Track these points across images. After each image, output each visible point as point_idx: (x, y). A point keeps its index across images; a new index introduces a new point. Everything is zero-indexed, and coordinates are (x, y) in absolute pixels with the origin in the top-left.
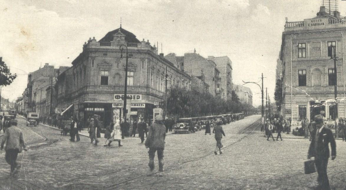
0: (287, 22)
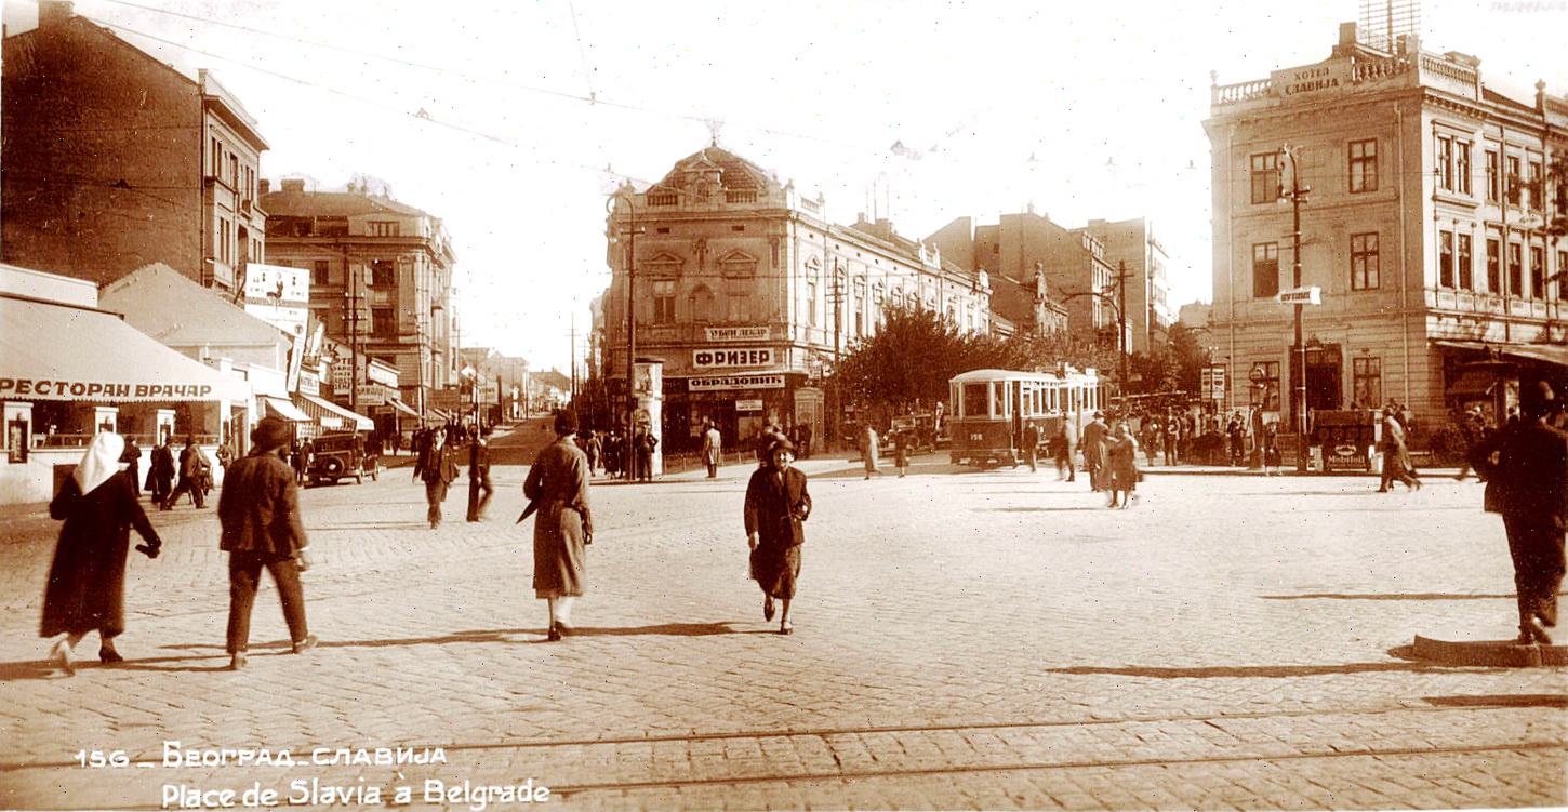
0: (1215, 88)
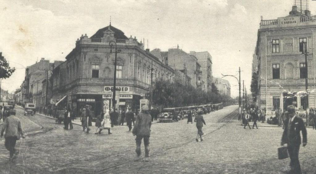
0: (262, 20)
